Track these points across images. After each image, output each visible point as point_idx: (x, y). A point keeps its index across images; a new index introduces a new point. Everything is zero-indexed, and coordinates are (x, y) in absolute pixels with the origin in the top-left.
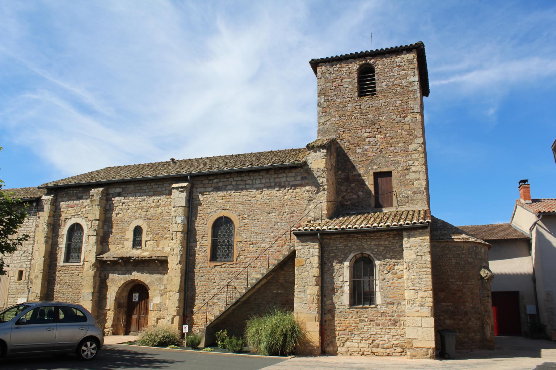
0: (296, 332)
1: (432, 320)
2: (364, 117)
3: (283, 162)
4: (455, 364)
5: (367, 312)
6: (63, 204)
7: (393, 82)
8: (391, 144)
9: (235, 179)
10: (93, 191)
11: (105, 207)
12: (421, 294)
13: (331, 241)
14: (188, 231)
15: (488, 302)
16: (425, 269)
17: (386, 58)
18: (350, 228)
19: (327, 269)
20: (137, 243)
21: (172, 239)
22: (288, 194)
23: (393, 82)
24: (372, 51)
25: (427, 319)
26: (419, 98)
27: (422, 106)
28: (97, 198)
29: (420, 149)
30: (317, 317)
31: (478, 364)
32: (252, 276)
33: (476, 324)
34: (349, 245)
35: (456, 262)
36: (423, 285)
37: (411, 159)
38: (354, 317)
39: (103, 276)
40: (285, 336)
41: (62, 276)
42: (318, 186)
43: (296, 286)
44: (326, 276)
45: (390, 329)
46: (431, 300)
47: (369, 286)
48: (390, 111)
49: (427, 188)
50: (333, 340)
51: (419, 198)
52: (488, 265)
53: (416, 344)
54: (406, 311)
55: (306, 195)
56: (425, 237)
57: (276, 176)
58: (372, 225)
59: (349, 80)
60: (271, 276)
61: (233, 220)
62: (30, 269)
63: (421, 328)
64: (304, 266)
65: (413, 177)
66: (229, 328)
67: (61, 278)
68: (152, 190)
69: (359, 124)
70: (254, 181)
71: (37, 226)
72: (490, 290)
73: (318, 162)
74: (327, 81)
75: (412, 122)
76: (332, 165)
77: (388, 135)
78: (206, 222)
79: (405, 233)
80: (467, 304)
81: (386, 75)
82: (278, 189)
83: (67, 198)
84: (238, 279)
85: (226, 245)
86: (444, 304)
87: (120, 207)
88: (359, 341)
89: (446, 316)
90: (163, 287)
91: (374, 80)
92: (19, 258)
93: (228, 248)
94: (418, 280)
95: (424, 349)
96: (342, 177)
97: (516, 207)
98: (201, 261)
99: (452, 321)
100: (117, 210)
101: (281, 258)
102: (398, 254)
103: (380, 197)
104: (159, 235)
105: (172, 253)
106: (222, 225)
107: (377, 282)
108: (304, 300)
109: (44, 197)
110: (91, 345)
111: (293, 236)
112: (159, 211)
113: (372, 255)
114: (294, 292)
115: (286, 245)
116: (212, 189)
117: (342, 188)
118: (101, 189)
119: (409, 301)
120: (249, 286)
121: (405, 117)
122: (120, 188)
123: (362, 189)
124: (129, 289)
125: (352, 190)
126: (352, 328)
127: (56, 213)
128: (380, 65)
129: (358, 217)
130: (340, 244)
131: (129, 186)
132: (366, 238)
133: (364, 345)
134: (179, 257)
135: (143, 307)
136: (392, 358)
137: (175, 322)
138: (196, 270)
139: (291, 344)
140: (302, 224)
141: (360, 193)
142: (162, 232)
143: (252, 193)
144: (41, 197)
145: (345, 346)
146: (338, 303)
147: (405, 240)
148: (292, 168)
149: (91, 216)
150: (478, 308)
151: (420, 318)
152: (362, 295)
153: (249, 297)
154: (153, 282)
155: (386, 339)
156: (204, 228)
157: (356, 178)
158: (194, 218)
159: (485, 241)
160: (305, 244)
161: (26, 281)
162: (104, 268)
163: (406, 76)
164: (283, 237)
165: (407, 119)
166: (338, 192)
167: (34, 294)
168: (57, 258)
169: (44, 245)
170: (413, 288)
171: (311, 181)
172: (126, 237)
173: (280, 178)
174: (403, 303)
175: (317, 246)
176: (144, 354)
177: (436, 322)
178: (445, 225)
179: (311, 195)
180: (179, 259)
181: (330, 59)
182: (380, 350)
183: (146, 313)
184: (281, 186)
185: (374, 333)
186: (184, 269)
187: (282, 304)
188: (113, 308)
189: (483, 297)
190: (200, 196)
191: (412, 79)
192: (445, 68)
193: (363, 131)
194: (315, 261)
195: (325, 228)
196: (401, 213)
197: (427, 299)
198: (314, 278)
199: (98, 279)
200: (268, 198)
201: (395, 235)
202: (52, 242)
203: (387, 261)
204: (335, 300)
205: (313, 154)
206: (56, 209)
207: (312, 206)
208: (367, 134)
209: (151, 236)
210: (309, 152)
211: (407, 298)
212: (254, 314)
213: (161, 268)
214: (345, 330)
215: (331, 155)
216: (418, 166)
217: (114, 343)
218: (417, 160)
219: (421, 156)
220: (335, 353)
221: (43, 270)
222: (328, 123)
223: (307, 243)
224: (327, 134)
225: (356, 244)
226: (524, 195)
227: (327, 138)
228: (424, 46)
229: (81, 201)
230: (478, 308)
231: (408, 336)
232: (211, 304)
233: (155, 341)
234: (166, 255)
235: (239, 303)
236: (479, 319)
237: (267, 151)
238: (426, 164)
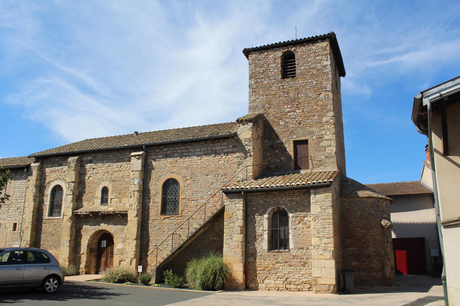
2: (286, 95)
4: (350, 297)
5: (282, 255)
6: (48, 170)
9: (180, 148)
10: (70, 159)
11: (80, 172)
12: (324, 240)
13: (254, 197)
14: (144, 190)
16: (328, 220)
17: (304, 46)
18: (267, 187)
20: (104, 201)
21: (131, 197)
22: (222, 160)
25: (329, 261)
28: (73, 165)
29: (331, 121)
30: (241, 259)
32: (194, 226)
33: (378, 265)
34: (268, 201)
36: (326, 233)
37: (324, 130)
38: (271, 259)
39: (78, 227)
40: (215, 274)
41: (46, 228)
42: (246, 153)
43: (225, 235)
44: (250, 226)
46: (332, 245)
47: (285, 234)
48: (308, 90)
50: (255, 278)
53: (320, 281)
54: (313, 254)
55: (236, 160)
56: (328, 194)
57: (212, 145)
59: (274, 65)
60: (208, 227)
61: (179, 181)
62: (22, 222)
63: (325, 269)
64: (231, 218)
65: (326, 144)
66: (174, 270)
67: (46, 228)
68: (115, 158)
69: (282, 101)
70: (195, 149)
71: (27, 188)
73: (245, 133)
74: (257, 66)
75: (325, 99)
76: (259, 135)
77: (305, 110)
78: (157, 183)
79: (312, 191)
80: (370, 249)
82: (214, 156)
83: (50, 165)
84: (182, 229)
85: (173, 201)
86: (350, 248)
87: (91, 172)
88: (275, 279)
89: (352, 259)
90: (124, 236)
91: (295, 64)
92: (14, 213)
93: (175, 204)
94: (322, 229)
95: (326, 286)
96: (268, 145)
98: (154, 214)
99: (357, 263)
100: (89, 174)
101: (215, 212)
102: (306, 207)
103: (299, 161)
104: (121, 194)
105: (131, 208)
106: (170, 185)
108: (231, 246)
109: (32, 165)
110: (53, 281)
111: (223, 194)
112: (121, 175)
113: (286, 209)
116: (162, 156)
117: (268, 154)
118: (76, 158)
119: (315, 246)
120: (190, 235)
121: (319, 95)
122: (91, 156)
123: (284, 155)
124: (99, 237)
125: (275, 155)
126: (270, 268)
127: (42, 177)
128: (299, 52)
131: (98, 155)
132: (282, 195)
133: (279, 282)
134: (136, 211)
135: (109, 252)
137: (133, 263)
138: (150, 222)
139: (220, 281)
141: (283, 158)
142: (123, 192)
143: (193, 159)
144: (31, 164)
145: (265, 283)
147: (312, 196)
149: (68, 180)
150: (379, 252)
151: (323, 260)
152: (278, 242)
153: (191, 243)
154: (116, 231)
155: (297, 278)
156: (156, 188)
158: (148, 180)
159: (387, 196)
160: (232, 200)
161: (19, 231)
162: (78, 220)
163: (320, 61)
166: (264, 157)
167: (25, 242)
168: (43, 213)
169: (32, 203)
170: (318, 236)
172: (96, 195)
173: (215, 147)
174: (310, 248)
175: (242, 202)
176: (96, 288)
179: (240, 161)
180: (136, 213)
181: (270, 46)
182: (292, 286)
183: (112, 257)
184: (216, 153)
185: (287, 272)
186: (140, 220)
188: (85, 252)
189: (383, 243)
190: (153, 162)
191: (325, 63)
193: (285, 107)
194: (240, 214)
197: (329, 244)
198: (239, 228)
199: (74, 229)
200: (206, 163)
201: (305, 193)
202: (39, 200)
203: (298, 213)
204: (257, 245)
205: (242, 126)
206: (42, 174)
207: (240, 170)
208: (288, 109)
209: (115, 194)
210: (238, 125)
211: (313, 244)
212: (195, 257)
213: (122, 220)
214: (264, 270)
217: (83, 281)
218: (328, 130)
219: (332, 126)
220: (256, 289)
221: (32, 222)
222: (257, 101)
225: (273, 200)
228: (335, 36)
229: (61, 167)
230: (379, 252)
232: (161, 249)
233: (115, 279)
234: (126, 210)
235: (183, 248)
236: (380, 261)
237: (211, 124)
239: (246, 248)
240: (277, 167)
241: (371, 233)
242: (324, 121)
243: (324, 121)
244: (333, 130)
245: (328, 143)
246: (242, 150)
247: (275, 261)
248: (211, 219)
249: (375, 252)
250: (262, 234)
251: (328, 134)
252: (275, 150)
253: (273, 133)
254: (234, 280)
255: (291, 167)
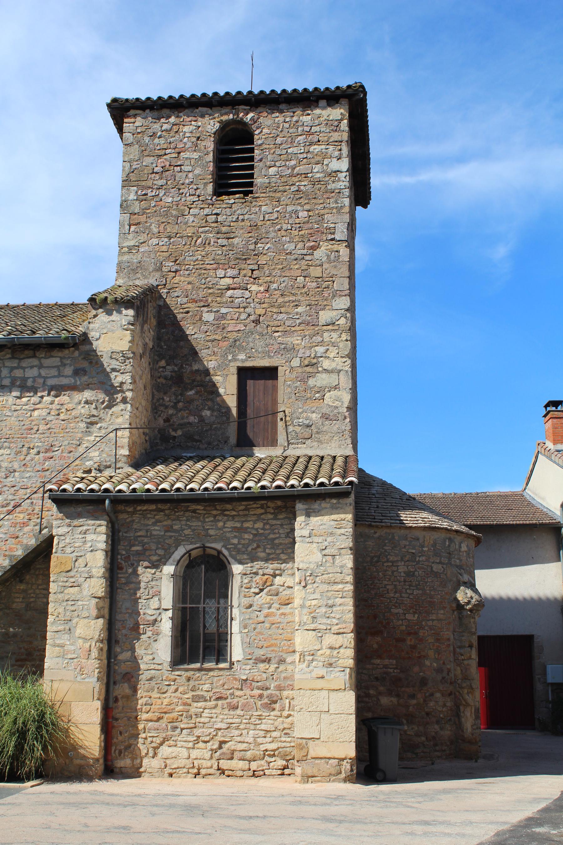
0: (46, 725)
1: (350, 698)
2: (225, 242)
3: (34, 333)
4: (397, 793)
5: (210, 679)
7: (293, 168)
8: (280, 307)
12: (330, 639)
13: (136, 517)
15: (470, 658)
16: (340, 586)
17: (281, 112)
18: (178, 490)
19: (123, 580)
22: (41, 407)
23: (293, 168)
24: (250, 92)
25: (340, 694)
26: (347, 209)
27: (352, 227)
29: (342, 321)
30: (97, 690)
31: (445, 791)
33: (445, 705)
35: (407, 570)
36: (335, 621)
38: (181, 689)
40: (22, 734)
42: (111, 391)
43: (50, 619)
44: (121, 596)
45: (260, 717)
46: (350, 653)
47: (218, 620)
49: (353, 408)
50: (132, 741)
51: (335, 428)
52: (474, 579)
54: (297, 676)
55: (84, 410)
56: (343, 516)
57: (15, 363)
58: (228, 484)
59: (195, 155)
63: (328, 716)
64: (72, 574)
65: (324, 383)
69: (211, 258)
72: (474, 634)
73: (113, 336)
74: (146, 153)
75: (329, 261)
76: (145, 345)
77: (275, 286)
79: (299, 506)
80: (427, 663)
81: (278, 152)
86: (378, 661)
88: (191, 745)
89: (381, 688)
91: (252, 159)
94: (323, 610)
95: (331, 761)
96: (168, 373)
97: (537, 457)
99: (394, 700)
101: (20, 553)
102: (285, 550)
107: (236, 612)
108: (69, 652)
111: (49, 503)
114: (46, 631)
115: (32, 523)
117: (167, 399)
119: (302, 655)
123: (210, 403)
126: (175, 715)
128: (267, 127)
129: (198, 466)
130: (154, 524)
132: (214, 512)
133: (202, 753)
136: (262, 782)
140: (71, 476)
141: (207, 413)
145: (159, 755)
146: (147, 658)
147: (300, 519)
148: (53, 346)
150: (449, 671)
152: (200, 640)
155: (251, 740)
157: (198, 378)
159: (470, 527)
160: (76, 522)
164: (26, 505)
165: (318, 254)
166: (156, 407)
170: (312, 626)
171: (95, 380)
173: (24, 368)
174: (289, 659)
175: (103, 529)
177: (359, 700)
178: (387, 489)
179: (95, 412)
181: (155, 102)
184: (26, 387)
185: (223, 726)
187: (17, 661)
189: (460, 647)
191: (335, 165)
192: (411, 149)
194: (98, 561)
195: (123, 487)
196: (293, 460)
197: (342, 650)
198: (94, 601)
203: (257, 565)
204: (140, 651)
205: (103, 317)
207: (96, 436)
208: (228, 281)
210: (94, 312)
211: (298, 648)
215: (145, 322)
216: (335, 360)
218: (334, 345)
219: (344, 336)
222: (142, 250)
223: (81, 521)
224: (139, 275)
225: (190, 527)
226: (554, 434)
227: (137, 282)
228: (365, 94)
230: (449, 671)
231: (297, 733)
236: (450, 694)
238: (353, 355)
239: (109, 658)
240: (189, 437)
241: (430, 623)
242: (322, 321)
243: (322, 321)
244: (346, 346)
245: (332, 379)
246: (103, 383)
247: (190, 695)
248: (6, 572)
249: (439, 670)
250: (156, 620)
251: (332, 355)
252: (187, 389)
253: (182, 343)
254: (75, 748)
255: (228, 438)
